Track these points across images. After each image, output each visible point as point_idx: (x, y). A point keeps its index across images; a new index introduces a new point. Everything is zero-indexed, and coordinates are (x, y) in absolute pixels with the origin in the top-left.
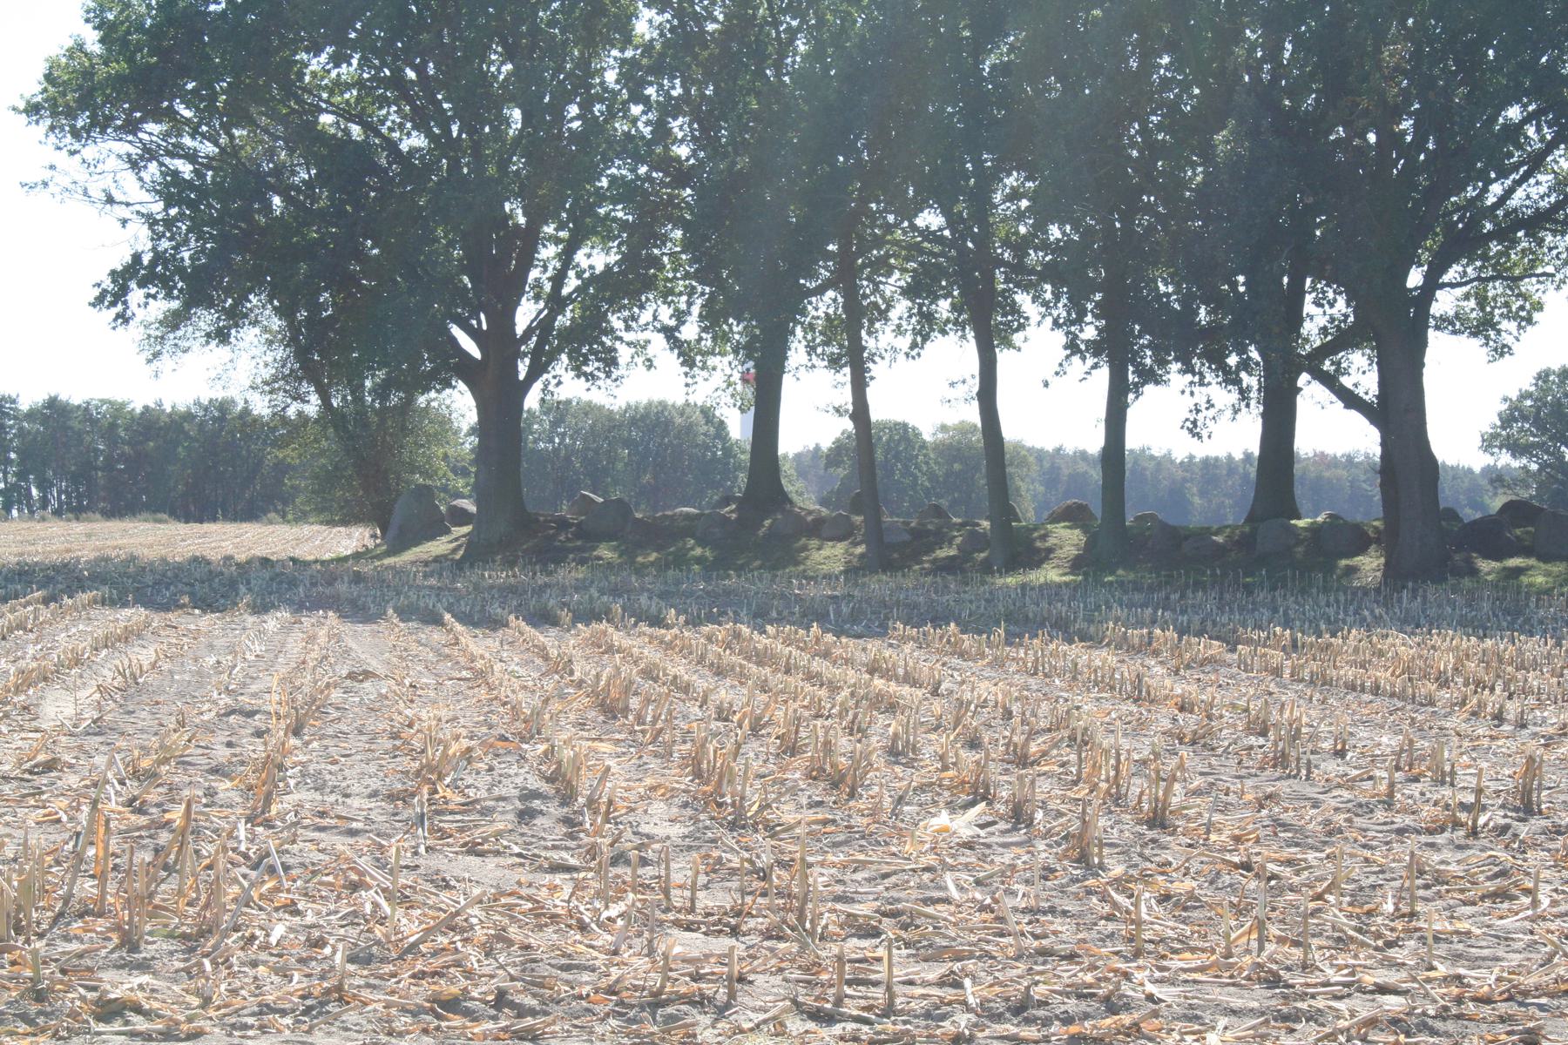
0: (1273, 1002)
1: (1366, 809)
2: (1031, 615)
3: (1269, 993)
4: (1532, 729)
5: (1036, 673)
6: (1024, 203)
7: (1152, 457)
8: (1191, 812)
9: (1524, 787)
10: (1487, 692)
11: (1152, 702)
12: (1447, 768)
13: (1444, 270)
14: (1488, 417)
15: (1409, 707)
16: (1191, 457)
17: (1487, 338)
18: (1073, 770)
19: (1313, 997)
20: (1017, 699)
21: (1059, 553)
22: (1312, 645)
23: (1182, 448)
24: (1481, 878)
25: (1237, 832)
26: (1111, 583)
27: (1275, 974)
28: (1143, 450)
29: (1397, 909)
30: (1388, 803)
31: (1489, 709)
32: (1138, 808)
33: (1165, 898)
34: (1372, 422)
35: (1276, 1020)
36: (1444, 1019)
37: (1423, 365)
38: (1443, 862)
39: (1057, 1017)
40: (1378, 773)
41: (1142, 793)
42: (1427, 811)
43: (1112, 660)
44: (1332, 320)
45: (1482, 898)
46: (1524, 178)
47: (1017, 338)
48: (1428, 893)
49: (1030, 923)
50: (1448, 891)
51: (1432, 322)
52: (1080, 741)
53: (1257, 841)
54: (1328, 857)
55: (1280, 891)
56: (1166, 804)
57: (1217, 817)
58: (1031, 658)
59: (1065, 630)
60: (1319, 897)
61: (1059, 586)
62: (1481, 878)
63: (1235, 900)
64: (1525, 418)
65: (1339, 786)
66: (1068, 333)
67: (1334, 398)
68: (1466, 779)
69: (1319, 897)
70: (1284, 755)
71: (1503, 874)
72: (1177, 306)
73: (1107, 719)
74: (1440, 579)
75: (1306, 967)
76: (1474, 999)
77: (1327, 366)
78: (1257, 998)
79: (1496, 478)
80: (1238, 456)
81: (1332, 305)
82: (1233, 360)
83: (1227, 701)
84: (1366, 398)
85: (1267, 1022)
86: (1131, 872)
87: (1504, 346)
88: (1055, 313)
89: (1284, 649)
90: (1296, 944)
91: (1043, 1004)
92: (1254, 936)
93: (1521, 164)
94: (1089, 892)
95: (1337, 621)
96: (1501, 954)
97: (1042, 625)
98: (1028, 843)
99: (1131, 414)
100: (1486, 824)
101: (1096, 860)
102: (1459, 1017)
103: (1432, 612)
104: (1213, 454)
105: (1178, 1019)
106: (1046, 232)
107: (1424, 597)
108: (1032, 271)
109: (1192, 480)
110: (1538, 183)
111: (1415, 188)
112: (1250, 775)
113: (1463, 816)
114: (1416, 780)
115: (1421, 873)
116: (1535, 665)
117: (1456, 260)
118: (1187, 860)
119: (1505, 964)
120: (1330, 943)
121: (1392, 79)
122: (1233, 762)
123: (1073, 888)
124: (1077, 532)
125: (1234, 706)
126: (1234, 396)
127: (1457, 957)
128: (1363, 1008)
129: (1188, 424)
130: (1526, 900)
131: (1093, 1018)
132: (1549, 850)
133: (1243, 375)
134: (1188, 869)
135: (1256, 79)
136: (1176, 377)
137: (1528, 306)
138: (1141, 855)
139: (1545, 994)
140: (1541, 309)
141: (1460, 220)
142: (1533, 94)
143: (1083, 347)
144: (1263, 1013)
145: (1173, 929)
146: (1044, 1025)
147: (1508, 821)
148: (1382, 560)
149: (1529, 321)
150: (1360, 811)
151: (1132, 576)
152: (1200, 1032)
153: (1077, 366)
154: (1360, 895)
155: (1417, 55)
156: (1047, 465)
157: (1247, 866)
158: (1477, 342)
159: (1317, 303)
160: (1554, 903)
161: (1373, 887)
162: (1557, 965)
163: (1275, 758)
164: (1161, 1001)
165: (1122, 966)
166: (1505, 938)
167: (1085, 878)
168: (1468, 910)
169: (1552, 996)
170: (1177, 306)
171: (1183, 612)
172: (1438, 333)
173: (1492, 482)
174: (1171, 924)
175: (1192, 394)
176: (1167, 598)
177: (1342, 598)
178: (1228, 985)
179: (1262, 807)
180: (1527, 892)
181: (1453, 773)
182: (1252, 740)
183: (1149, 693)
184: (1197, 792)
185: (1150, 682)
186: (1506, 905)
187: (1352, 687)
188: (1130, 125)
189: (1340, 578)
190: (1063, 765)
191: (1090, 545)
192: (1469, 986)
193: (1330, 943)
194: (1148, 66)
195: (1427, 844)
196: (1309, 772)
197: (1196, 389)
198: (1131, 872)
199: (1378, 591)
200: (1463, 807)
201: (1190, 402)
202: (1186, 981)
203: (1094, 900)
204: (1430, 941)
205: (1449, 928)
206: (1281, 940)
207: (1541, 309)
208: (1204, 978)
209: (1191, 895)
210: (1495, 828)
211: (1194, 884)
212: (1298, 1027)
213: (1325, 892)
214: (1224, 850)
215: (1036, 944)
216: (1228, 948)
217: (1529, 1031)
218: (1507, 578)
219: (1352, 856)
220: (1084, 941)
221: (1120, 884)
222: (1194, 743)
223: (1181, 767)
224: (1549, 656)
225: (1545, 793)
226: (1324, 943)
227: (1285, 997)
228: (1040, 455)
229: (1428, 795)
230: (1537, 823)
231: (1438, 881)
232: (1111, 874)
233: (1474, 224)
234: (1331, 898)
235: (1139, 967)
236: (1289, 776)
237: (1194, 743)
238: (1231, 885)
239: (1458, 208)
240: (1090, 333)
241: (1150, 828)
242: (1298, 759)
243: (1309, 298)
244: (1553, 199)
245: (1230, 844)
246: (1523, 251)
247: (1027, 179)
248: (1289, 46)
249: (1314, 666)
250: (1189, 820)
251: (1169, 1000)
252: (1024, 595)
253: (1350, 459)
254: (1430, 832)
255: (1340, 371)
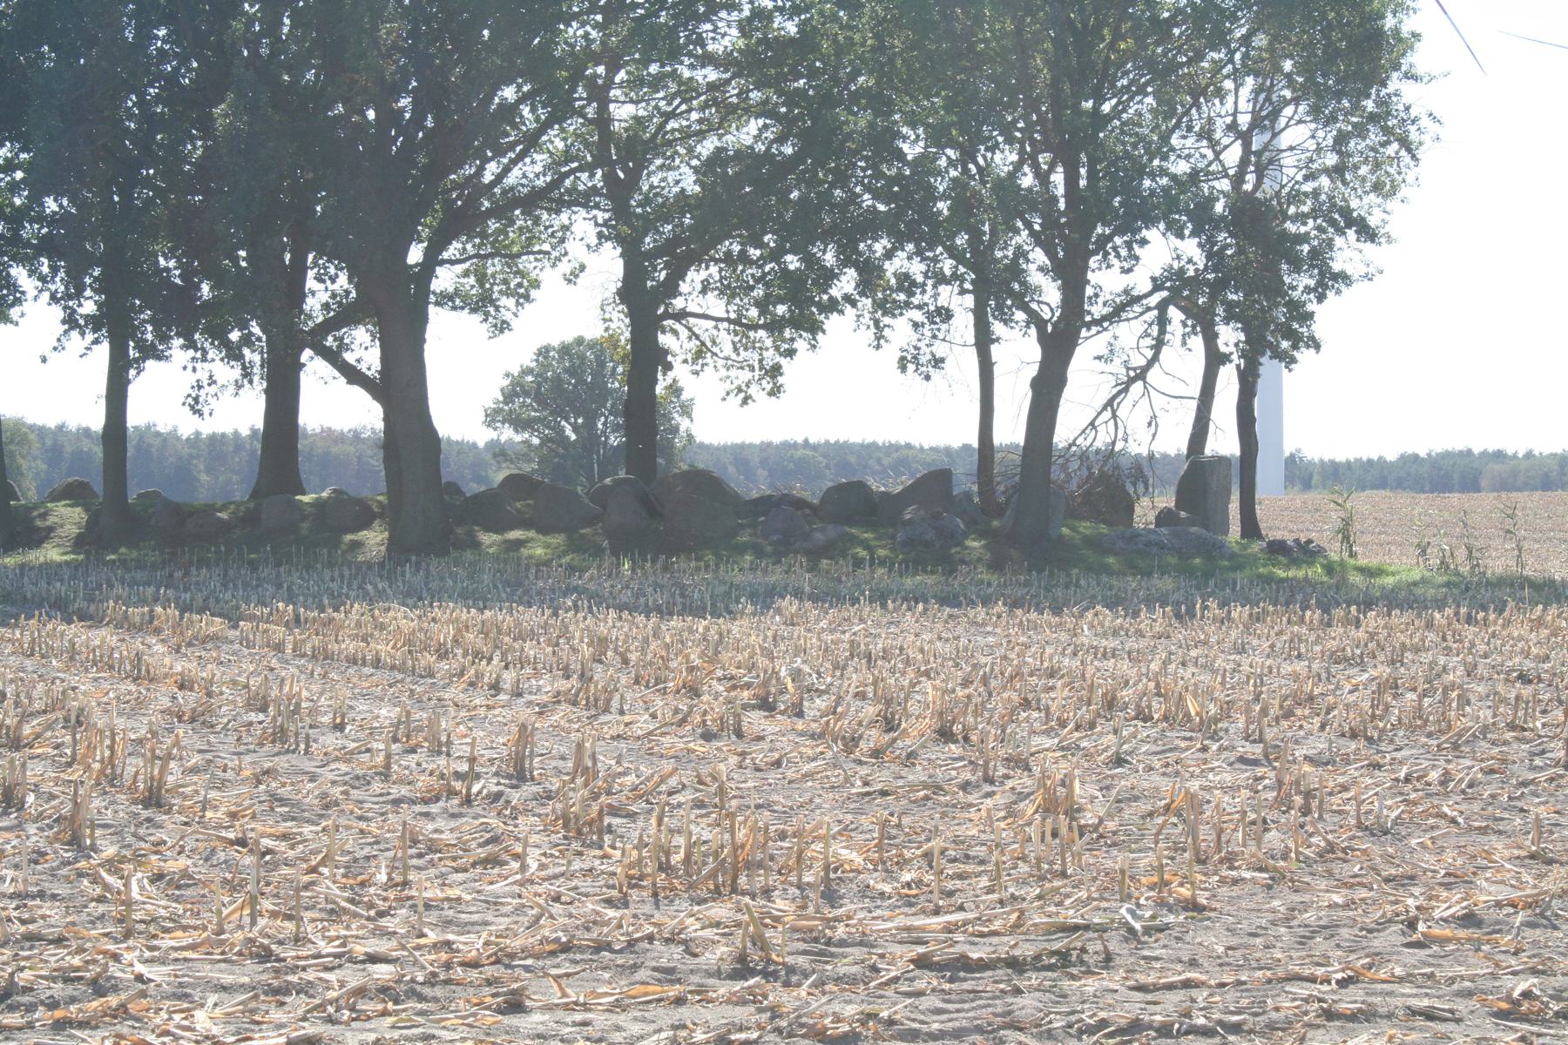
0: (264, 977)
1: (362, 781)
2: (29, 595)
3: (260, 968)
4: (528, 697)
5: (32, 655)
6: (19, 175)
7: (158, 434)
8: (188, 790)
9: (517, 754)
10: (484, 662)
11: (151, 681)
12: (444, 739)
13: (444, 247)
14: (491, 393)
15: (408, 680)
16: (198, 434)
17: (487, 314)
18: (68, 751)
19: (304, 969)
20: (12, 681)
21: (59, 531)
22: (314, 620)
23: (187, 426)
24: (473, 845)
25: (233, 808)
26: (113, 561)
27: (267, 949)
28: (148, 427)
29: (390, 879)
30: (385, 774)
31: (486, 680)
32: (133, 788)
33: (157, 878)
34: (375, 397)
35: (266, 993)
36: (433, 985)
37: (424, 341)
38: (436, 831)
39: (42, 1003)
40: (375, 745)
41: (137, 773)
42: (423, 781)
43: (113, 640)
44: (334, 296)
45: (474, 865)
46: (520, 157)
47: (14, 312)
48: (420, 862)
49: (17, 908)
50: (440, 859)
51: (432, 298)
52: (77, 722)
53: (254, 817)
54: (324, 830)
55: (275, 865)
56: (161, 783)
57: (213, 794)
58: (27, 639)
59: (64, 609)
60: (314, 870)
61: (60, 565)
62: (473, 845)
63: (229, 876)
64: (526, 394)
65: (337, 759)
66: (65, 308)
67: (337, 374)
68: (461, 748)
69: (314, 870)
70: (283, 730)
71: (494, 840)
72: (178, 281)
73: (105, 699)
74: (444, 553)
75: (298, 940)
76: (463, 964)
77: (330, 341)
78: (248, 973)
79: (499, 452)
80: (245, 432)
81: (333, 281)
82: (235, 336)
83: (227, 678)
84: (369, 373)
85: (256, 997)
86: (124, 852)
87: (504, 322)
88: (53, 287)
89: (287, 625)
90: (289, 918)
91: (27, 990)
92: (247, 911)
93: (516, 143)
94: (80, 875)
95: (340, 595)
96: (490, 918)
97: (40, 606)
98: (19, 826)
99: (133, 391)
100: (480, 792)
101: (88, 842)
102: (447, 982)
103: (434, 585)
104: (219, 430)
105: (167, 998)
106: (42, 205)
107: (428, 571)
108: (28, 244)
109: (198, 457)
110: (533, 162)
111: (414, 165)
112: (249, 751)
113: (458, 785)
114: (413, 751)
115: (415, 842)
116: (532, 635)
117: (456, 237)
118: (182, 838)
119: (493, 928)
120: (323, 915)
121: (390, 56)
122: (232, 739)
123: (65, 871)
124: (78, 509)
125: (234, 683)
126: (237, 372)
127: (447, 923)
128: (353, 977)
129: (190, 400)
130: (515, 865)
131: (80, 1001)
132: (539, 816)
133: (246, 352)
134: (182, 847)
135: (255, 54)
136: (178, 353)
137: (526, 283)
138: (135, 835)
139: (531, 956)
140: (538, 287)
141: (458, 198)
142: (528, 75)
143: (82, 322)
144: (254, 988)
145: (165, 908)
146: (27, 1011)
147: (501, 788)
148: (386, 534)
149: (527, 297)
150: (357, 783)
151: (135, 554)
152: (188, 1010)
153: (76, 341)
154: (356, 869)
155: (414, 33)
156: (49, 442)
157: (242, 842)
158: (478, 317)
159: (319, 279)
160: (542, 867)
161: (368, 858)
162: (542, 927)
163: (274, 734)
164: (150, 980)
165: (112, 947)
166: (494, 903)
167: (76, 860)
168: (460, 877)
169: (537, 957)
170: (178, 281)
171: (187, 589)
172: (438, 309)
173: (495, 456)
174: (163, 903)
175: (194, 370)
176: (171, 576)
177: (346, 573)
178: (219, 961)
179: (259, 782)
180: (516, 857)
181: (449, 743)
182: (253, 717)
183: (148, 672)
184: (194, 770)
185: (150, 660)
186: (496, 871)
187: (353, 661)
188: (128, 98)
189: (344, 553)
190: (57, 747)
191: (92, 524)
192: (458, 951)
193: (323, 915)
194: (144, 36)
195: (421, 814)
196: (308, 746)
197: (199, 365)
198: (124, 852)
199: (382, 565)
200: (458, 775)
201: (191, 379)
202: (177, 960)
203: (85, 882)
204: (421, 908)
205: (441, 895)
206: (274, 915)
207: (538, 287)
208: (195, 956)
209: (185, 874)
210: (488, 796)
211: (189, 862)
212: (288, 1000)
213: (319, 865)
214: (220, 827)
215: (23, 929)
216: (220, 924)
217: (513, 992)
218: (508, 550)
219: (348, 828)
220: (73, 924)
221: (112, 865)
222: (193, 720)
223: (177, 744)
224: (546, 626)
225: (537, 759)
226: (318, 915)
227: (277, 971)
228: (42, 431)
229: (424, 765)
230: (529, 789)
231: (431, 850)
232: (103, 855)
233: (471, 202)
234: (325, 871)
235: (128, 948)
236: (288, 751)
237: (193, 720)
238: (226, 862)
239: (456, 185)
240: (89, 307)
241: (146, 808)
242: (297, 734)
243: (311, 274)
244: (548, 179)
245: (226, 821)
246: (520, 228)
247: (22, 150)
248: (287, 21)
249: (316, 640)
250: (185, 797)
251: (159, 979)
252: (22, 575)
253: (356, 435)
254: (426, 801)
255: (342, 346)
